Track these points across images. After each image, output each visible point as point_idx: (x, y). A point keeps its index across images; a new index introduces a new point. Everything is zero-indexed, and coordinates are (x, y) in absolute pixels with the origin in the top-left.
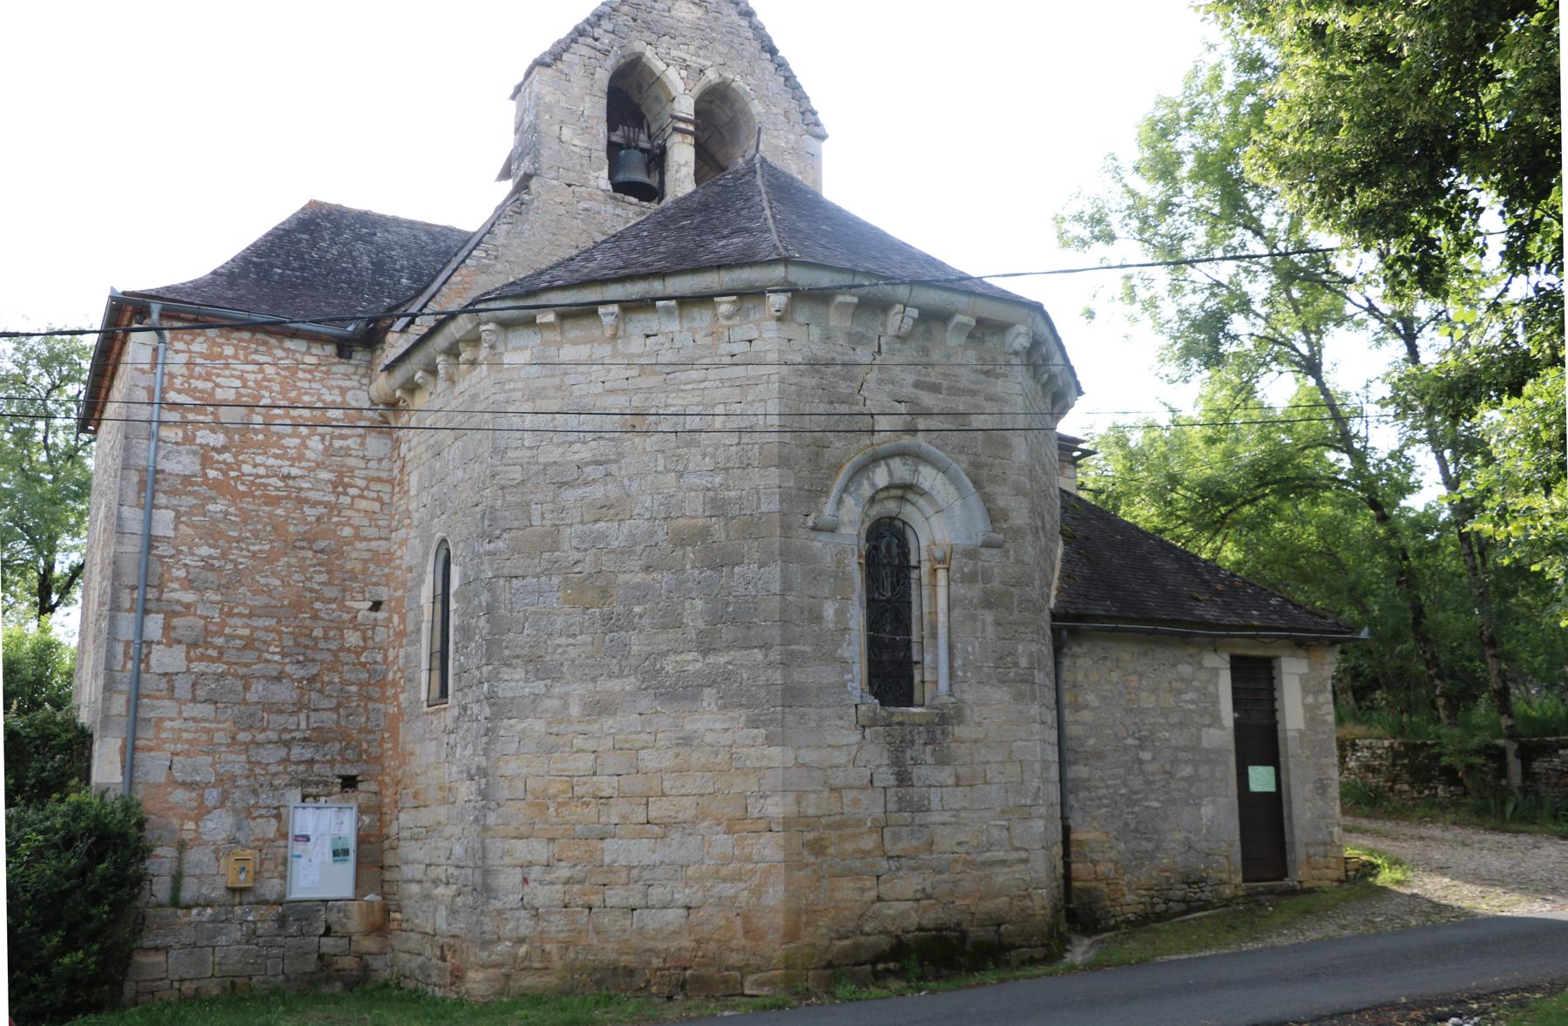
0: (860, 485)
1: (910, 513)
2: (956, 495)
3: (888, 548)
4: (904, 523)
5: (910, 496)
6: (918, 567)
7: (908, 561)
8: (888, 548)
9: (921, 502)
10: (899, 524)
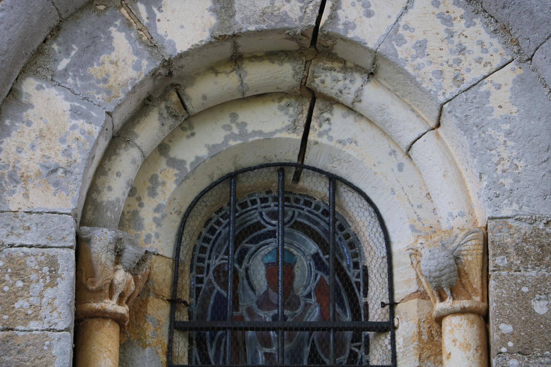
0: (96, 46)
1: (345, 144)
2: (497, 50)
3: (282, 271)
4: (334, 180)
5: (329, 80)
6: (388, 328)
7: (359, 311)
8: (282, 271)
9: (373, 95)
10: (319, 188)
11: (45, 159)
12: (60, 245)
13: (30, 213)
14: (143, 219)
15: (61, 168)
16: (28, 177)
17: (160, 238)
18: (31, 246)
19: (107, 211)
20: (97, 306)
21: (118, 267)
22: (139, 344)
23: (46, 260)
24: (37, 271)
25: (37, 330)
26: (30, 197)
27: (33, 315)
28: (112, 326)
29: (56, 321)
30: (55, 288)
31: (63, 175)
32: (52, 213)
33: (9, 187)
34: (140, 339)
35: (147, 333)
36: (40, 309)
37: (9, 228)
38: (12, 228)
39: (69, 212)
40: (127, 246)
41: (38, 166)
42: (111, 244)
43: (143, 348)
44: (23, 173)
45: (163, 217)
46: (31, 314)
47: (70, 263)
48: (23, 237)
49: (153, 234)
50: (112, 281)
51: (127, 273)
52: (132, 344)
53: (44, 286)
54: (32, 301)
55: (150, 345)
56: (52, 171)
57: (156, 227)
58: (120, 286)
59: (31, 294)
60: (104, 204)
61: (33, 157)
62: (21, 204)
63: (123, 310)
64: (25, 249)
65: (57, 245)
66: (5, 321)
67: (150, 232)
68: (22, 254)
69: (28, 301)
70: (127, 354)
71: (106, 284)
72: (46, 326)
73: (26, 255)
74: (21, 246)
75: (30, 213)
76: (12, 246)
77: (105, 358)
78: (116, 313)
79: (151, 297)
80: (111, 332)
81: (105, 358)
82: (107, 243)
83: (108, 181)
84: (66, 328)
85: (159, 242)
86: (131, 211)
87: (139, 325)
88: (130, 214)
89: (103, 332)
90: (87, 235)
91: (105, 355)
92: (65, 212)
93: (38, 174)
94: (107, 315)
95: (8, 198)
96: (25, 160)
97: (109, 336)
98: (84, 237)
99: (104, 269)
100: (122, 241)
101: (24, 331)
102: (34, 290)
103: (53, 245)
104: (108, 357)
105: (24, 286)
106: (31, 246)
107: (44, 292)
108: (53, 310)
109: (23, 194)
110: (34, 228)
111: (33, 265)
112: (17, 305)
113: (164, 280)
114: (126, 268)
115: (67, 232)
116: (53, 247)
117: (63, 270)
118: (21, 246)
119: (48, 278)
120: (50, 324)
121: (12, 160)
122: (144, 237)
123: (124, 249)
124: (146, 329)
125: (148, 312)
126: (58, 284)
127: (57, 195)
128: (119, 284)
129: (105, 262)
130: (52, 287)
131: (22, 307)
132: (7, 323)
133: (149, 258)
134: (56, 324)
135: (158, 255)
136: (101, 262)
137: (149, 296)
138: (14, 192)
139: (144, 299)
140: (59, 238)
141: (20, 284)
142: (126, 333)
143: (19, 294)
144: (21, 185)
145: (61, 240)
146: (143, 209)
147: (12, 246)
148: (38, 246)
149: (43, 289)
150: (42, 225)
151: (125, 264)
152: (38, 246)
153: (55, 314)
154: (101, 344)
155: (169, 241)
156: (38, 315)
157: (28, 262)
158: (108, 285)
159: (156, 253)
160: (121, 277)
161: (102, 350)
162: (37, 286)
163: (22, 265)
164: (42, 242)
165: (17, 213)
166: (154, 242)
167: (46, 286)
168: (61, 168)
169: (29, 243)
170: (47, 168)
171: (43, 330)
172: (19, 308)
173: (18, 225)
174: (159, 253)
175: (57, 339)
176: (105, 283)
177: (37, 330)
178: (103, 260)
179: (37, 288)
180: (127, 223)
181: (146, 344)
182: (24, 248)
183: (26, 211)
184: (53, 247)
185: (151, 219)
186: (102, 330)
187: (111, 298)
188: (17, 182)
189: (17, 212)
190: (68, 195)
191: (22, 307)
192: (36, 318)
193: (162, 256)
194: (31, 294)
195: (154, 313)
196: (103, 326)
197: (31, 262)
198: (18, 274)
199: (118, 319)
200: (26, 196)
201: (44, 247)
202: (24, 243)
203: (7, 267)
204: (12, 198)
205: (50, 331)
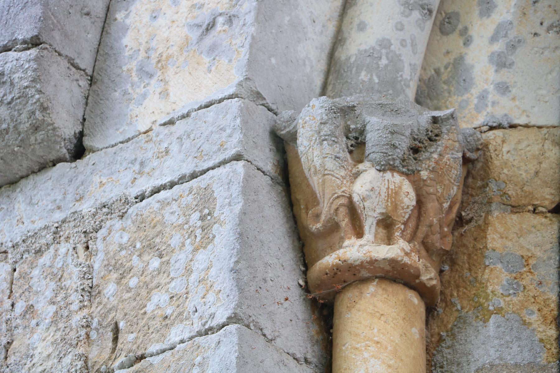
11: (196, 12)
12: (217, 161)
13: (171, 122)
14: (473, 66)
15: (221, 14)
16: (169, 57)
17: (514, 91)
18: (172, 185)
19: (358, 73)
20: (330, 260)
21: (361, 167)
22: (477, 317)
23: (195, 199)
24: (181, 226)
25: (182, 342)
26: (171, 94)
27: (175, 314)
28: (380, 291)
29: (212, 310)
30: (210, 247)
31: (226, 27)
32: (207, 106)
33: (138, 90)
34: (478, 306)
35: (490, 288)
36: (187, 298)
37: (137, 167)
38: (142, 164)
39: (231, 91)
40: (368, 118)
41: (186, 29)
42: (325, 123)
43: (484, 322)
44: (161, 55)
45: (513, 47)
46: (172, 315)
47: (234, 187)
48: (157, 173)
49: (491, 88)
50: (350, 198)
51: (388, 175)
52: (465, 322)
53: (193, 251)
54: (174, 288)
55: (499, 311)
56: (207, 30)
57: (496, 71)
58: (367, 204)
59: (172, 276)
60: (352, 60)
61: (175, 17)
62: (156, 112)
63: (398, 250)
64: (163, 194)
65: (210, 164)
66: (130, 345)
67: (486, 87)
68: (157, 205)
69: (167, 291)
70: (458, 347)
71: (337, 210)
72: (197, 326)
73: (165, 204)
74: (156, 191)
75: (171, 122)
76: (141, 198)
77: (365, 360)
78: (373, 262)
79: (496, 213)
80: (380, 305)
81: (365, 360)
82: (315, 125)
83: (358, 13)
84: (229, 318)
85: (514, 99)
86: (452, 61)
87: (476, 278)
88: (449, 69)
89: (359, 311)
90: (289, 126)
91: (366, 355)
92: (227, 94)
93: (185, 44)
94: (365, 274)
95: (136, 111)
96: (164, 30)
97: (372, 315)
98: (282, 132)
99: (324, 181)
100: (358, 112)
101: (163, 351)
102: (177, 265)
103: (205, 167)
104: (373, 356)
105: (162, 263)
106: (172, 185)
107: (192, 263)
108: (208, 291)
109: (160, 93)
110: (175, 148)
111: (174, 218)
112: (150, 308)
113: (537, 173)
114: (379, 164)
115: (228, 131)
116: (208, 170)
117: (222, 207)
118: (156, 191)
119: (198, 232)
120: (204, 321)
121: (143, 40)
122: (476, 101)
123: (365, 126)
124: (488, 281)
125: (490, 246)
126: (214, 237)
127: (213, 68)
128: (364, 200)
129: (323, 165)
130: (205, 248)
131: (158, 307)
132: (134, 347)
133: (444, 130)
134: (212, 316)
135: (512, 126)
136: (315, 167)
137: (489, 213)
138: (144, 96)
139: (481, 222)
140: (215, 148)
141: (155, 263)
142: (454, 305)
143: (152, 285)
144: (156, 78)
145: (219, 150)
146: (472, 47)
147: (141, 198)
148: (182, 180)
149: (190, 256)
150: (189, 136)
151: (373, 156)
152: (182, 180)
153: (211, 297)
154: (356, 335)
155: (544, 92)
156: (183, 312)
157: (167, 216)
158: (343, 211)
159: (505, 124)
160: (370, 186)
161: (358, 346)
162: (182, 256)
163: (158, 226)
164: (187, 170)
165: (150, 133)
166: (494, 103)
167: (196, 250)
168: (221, 14)
169: (166, 180)
170: (199, 26)
171: (191, 338)
172: (153, 311)
173: (150, 154)
174: (516, 122)
175: (213, 345)
176: (334, 207)
177: (182, 342)
178: (317, 162)
179: (180, 259)
180: (446, 87)
181: (489, 311)
182: (162, 192)
183: (163, 122)
184: (208, 170)
185: (486, 59)
186: (358, 306)
187: (359, 234)
188: (151, 76)
189: (150, 130)
190: (230, 61)
191: (158, 307)
192: (180, 317)
193: (527, 126)
194: (172, 276)
195: (509, 244)
196: (361, 299)
197: (172, 215)
198: (151, 247)
199: (395, 275)
200: (165, 94)
201: (194, 176)
202: (159, 182)
203: (135, 239)
204: (141, 108)
205: (206, 333)
